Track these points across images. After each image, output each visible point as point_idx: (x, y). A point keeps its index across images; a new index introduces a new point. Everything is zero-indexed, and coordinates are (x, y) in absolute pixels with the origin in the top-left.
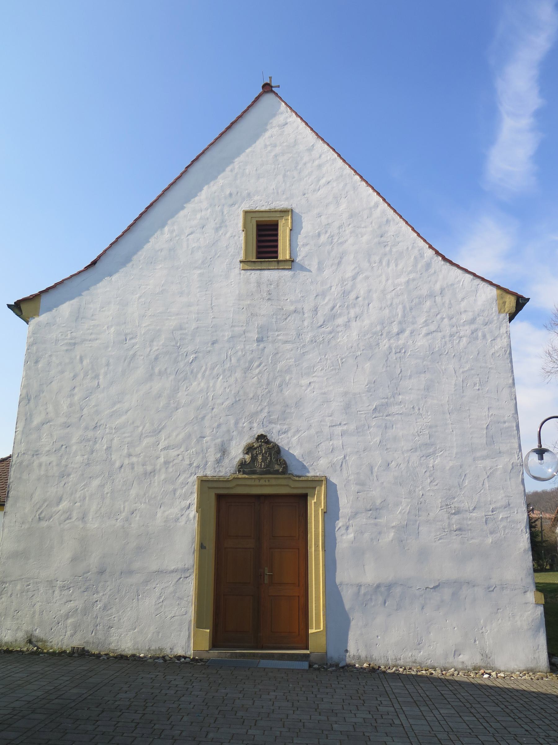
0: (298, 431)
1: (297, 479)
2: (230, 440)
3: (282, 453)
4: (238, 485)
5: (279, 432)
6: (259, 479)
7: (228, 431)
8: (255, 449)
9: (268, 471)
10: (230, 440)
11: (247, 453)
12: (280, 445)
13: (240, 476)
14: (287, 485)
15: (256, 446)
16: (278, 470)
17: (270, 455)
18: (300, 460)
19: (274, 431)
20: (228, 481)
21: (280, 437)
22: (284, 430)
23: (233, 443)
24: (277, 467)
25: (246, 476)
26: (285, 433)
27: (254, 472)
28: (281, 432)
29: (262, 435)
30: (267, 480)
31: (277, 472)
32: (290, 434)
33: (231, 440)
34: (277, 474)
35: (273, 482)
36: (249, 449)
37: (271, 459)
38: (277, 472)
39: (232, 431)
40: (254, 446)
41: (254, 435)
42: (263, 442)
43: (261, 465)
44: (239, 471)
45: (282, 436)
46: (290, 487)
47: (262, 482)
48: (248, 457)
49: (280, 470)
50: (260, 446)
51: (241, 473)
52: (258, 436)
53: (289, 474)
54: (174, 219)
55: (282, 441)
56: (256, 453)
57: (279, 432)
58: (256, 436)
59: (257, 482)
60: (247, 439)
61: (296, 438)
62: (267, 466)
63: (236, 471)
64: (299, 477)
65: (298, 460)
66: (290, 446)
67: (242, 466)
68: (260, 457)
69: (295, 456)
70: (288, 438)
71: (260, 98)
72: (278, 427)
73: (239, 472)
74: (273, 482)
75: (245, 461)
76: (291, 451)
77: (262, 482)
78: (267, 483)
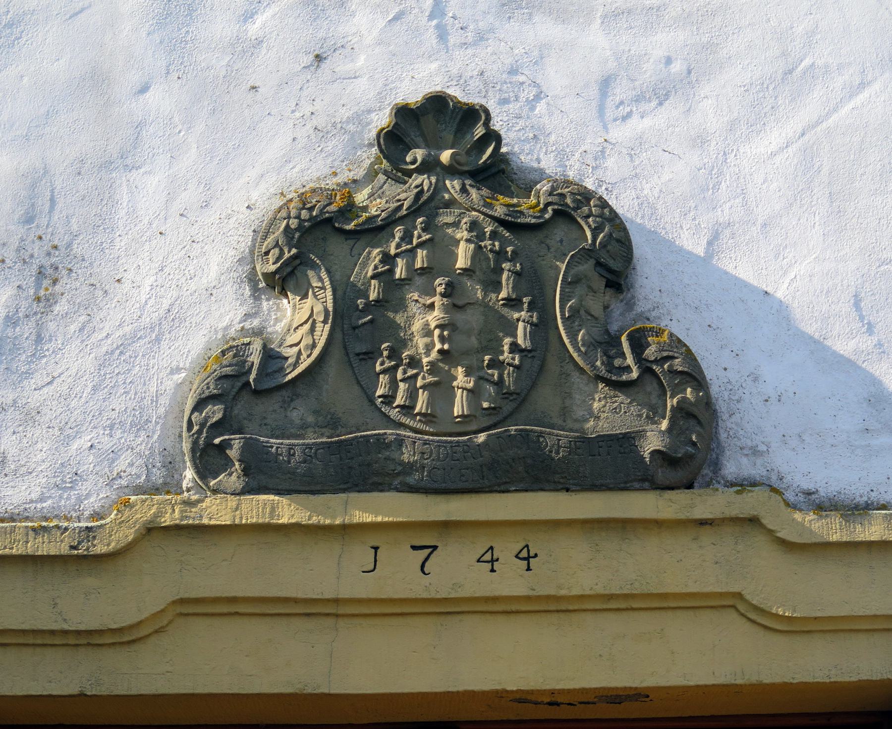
0: (793, 75)
1: (834, 530)
2: (107, 165)
3: (650, 280)
4: (190, 608)
5: (606, 84)
6: (427, 540)
7: (95, 81)
8: (375, 231)
9: (515, 456)
10: (107, 165)
11: (284, 280)
12: (623, 204)
13: (217, 510)
14: (731, 603)
15: (377, 208)
16: (626, 442)
17: (533, 289)
18: (844, 347)
19: (555, 79)
20: (80, 562)
21: (620, 133)
22: (649, 72)
23: (146, 192)
24: (605, 413)
25: (288, 510)
26: (661, 94)
27: (355, 467)
28: (620, 91)
29: (437, 103)
30: (507, 549)
31: (610, 464)
32: (711, 107)
33: (122, 160)
34: (623, 486)
35: (575, 567)
36: (311, 238)
37: (543, 327)
38: (610, 464)
39: (134, 78)
40: (349, 209)
41: (359, 118)
42: (452, 170)
43: (441, 388)
44: (208, 459)
45: (636, 125)
46: (761, 619)
47: (457, 570)
48: (296, 324)
49: (653, 441)
50: (426, 207)
51: (233, 479)
52: (403, 112)
53: (744, 485)
54: (791, 681)
55: (648, 175)
56: (385, 276)
57: (606, 84)
58: (383, 119)
59: (400, 574)
60: (310, 141)
61: (773, 138)
62: (510, 403)
63: (171, 466)
64: (857, 510)
65: (817, 349)
66: (723, 214)
67: (240, 405)
68: (424, 321)
69: (780, 313)
70: (700, 141)
71: (522, 615)
72: (596, 45)
73: (205, 471)
74: (575, 567)
75: (270, 356)
76: (741, 265)
77: (457, 570)
78: (510, 581)
